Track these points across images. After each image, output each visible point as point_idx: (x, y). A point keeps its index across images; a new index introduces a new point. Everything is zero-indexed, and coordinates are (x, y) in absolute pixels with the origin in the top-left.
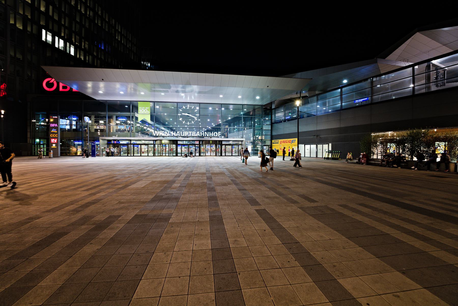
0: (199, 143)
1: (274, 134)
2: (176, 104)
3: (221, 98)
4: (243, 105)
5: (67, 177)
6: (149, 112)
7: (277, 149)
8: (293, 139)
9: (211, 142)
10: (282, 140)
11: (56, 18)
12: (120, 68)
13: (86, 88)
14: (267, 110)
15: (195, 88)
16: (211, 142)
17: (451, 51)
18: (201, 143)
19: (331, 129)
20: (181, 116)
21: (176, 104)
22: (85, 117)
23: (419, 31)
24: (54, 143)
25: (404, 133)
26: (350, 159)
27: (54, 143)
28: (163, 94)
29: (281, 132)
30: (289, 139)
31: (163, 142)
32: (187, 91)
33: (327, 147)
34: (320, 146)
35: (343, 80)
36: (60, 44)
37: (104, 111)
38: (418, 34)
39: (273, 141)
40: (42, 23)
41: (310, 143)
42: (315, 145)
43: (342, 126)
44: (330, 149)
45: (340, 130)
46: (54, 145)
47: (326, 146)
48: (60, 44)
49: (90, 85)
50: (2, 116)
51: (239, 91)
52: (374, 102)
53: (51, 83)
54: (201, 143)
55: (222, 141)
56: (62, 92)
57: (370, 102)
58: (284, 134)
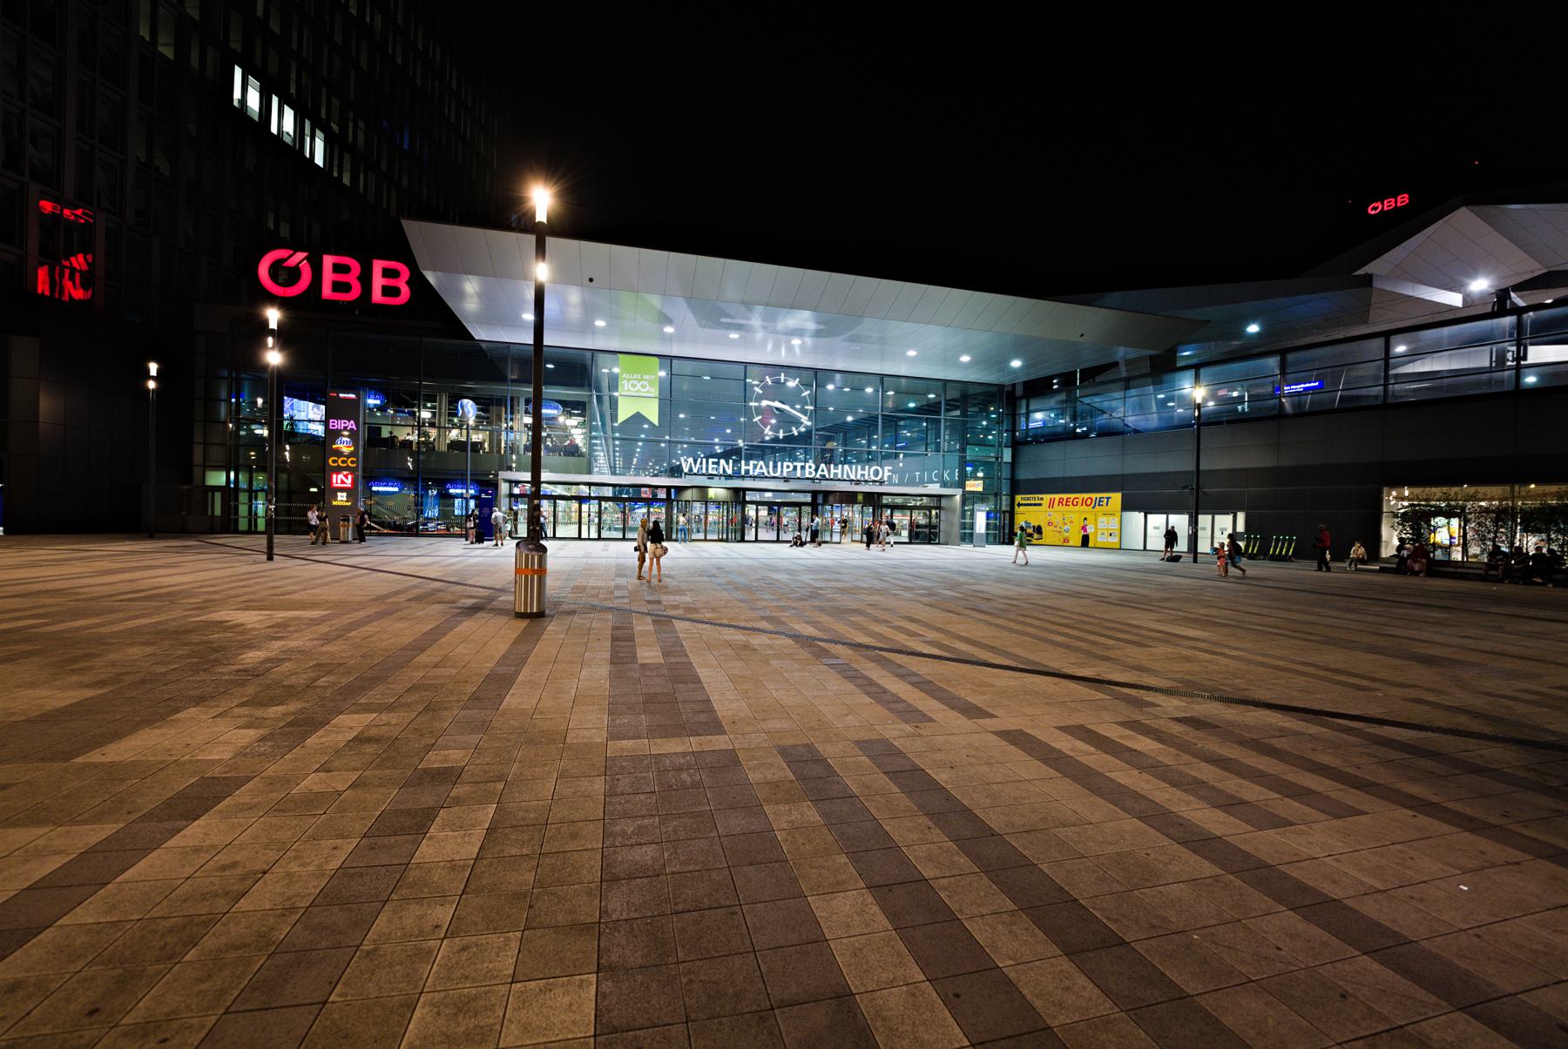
0: (669, 494)
1: (1023, 474)
2: (742, 367)
3: (604, 331)
6: (655, 392)
9: (860, 498)
11: (275, 26)
12: (454, 223)
13: (461, 294)
14: (1009, 398)
15: (803, 319)
16: (860, 498)
17: (1538, 269)
18: (820, 500)
20: (759, 410)
21: (742, 367)
22: (465, 401)
23: (1468, 203)
24: (342, 490)
25: (198, 438)
26: (1362, 561)
27: (342, 490)
28: (734, 336)
29: (1054, 472)
30: (1086, 496)
31: (712, 493)
32: (782, 328)
33: (1221, 528)
34: (1204, 520)
35: (1248, 324)
36: (285, 122)
38: (1463, 209)
39: (1018, 498)
40: (236, 46)
43: (1286, 461)
44: (1241, 528)
45: (1275, 475)
46: (342, 496)
47: (1224, 522)
48: (285, 122)
49: (471, 286)
50: (152, 385)
51: (931, 335)
52: (1391, 401)
53: (289, 268)
54: (820, 500)
56: (379, 306)
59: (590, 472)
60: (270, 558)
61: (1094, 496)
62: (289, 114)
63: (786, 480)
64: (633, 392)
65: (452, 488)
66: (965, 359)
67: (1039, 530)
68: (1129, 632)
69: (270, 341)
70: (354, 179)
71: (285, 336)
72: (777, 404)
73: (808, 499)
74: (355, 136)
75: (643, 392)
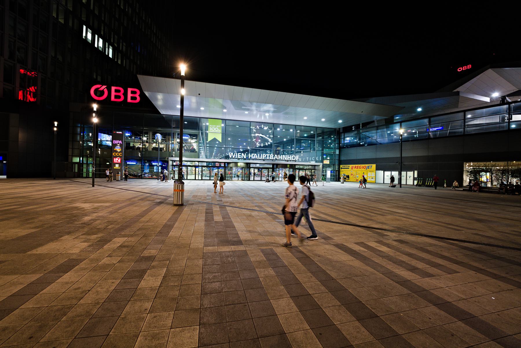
0: (225, 165)
1: (342, 158)
3: (204, 111)
4: (250, 122)
5: (103, 203)
6: (220, 131)
7: (347, 174)
8: (368, 165)
9: (288, 166)
10: (354, 165)
11: (97, 12)
12: (154, 76)
14: (338, 133)
15: (270, 107)
16: (288, 166)
18: (275, 167)
19: (418, 157)
20: (255, 137)
22: (158, 134)
23: (492, 67)
24: (117, 163)
26: (457, 187)
27: (117, 163)
28: (247, 112)
31: (239, 164)
32: (262, 110)
35: (418, 108)
36: (100, 43)
37: (170, 127)
38: (490, 72)
39: (341, 166)
40: (84, 19)
41: (391, 169)
42: (397, 172)
43: (431, 154)
44: (416, 176)
45: (427, 158)
46: (117, 166)
47: (410, 174)
48: (100, 43)
49: (160, 96)
50: (55, 129)
51: (312, 112)
52: (466, 133)
53: (101, 91)
54: (275, 167)
55: (250, 163)
57: (462, 134)
58: (356, 160)
60: (93, 186)
61: (366, 165)
62: (101, 41)
64: (213, 131)
65: (150, 162)
66: (323, 120)
69: (94, 115)
70: (122, 62)
71: (99, 113)
73: (271, 166)
75: (217, 131)
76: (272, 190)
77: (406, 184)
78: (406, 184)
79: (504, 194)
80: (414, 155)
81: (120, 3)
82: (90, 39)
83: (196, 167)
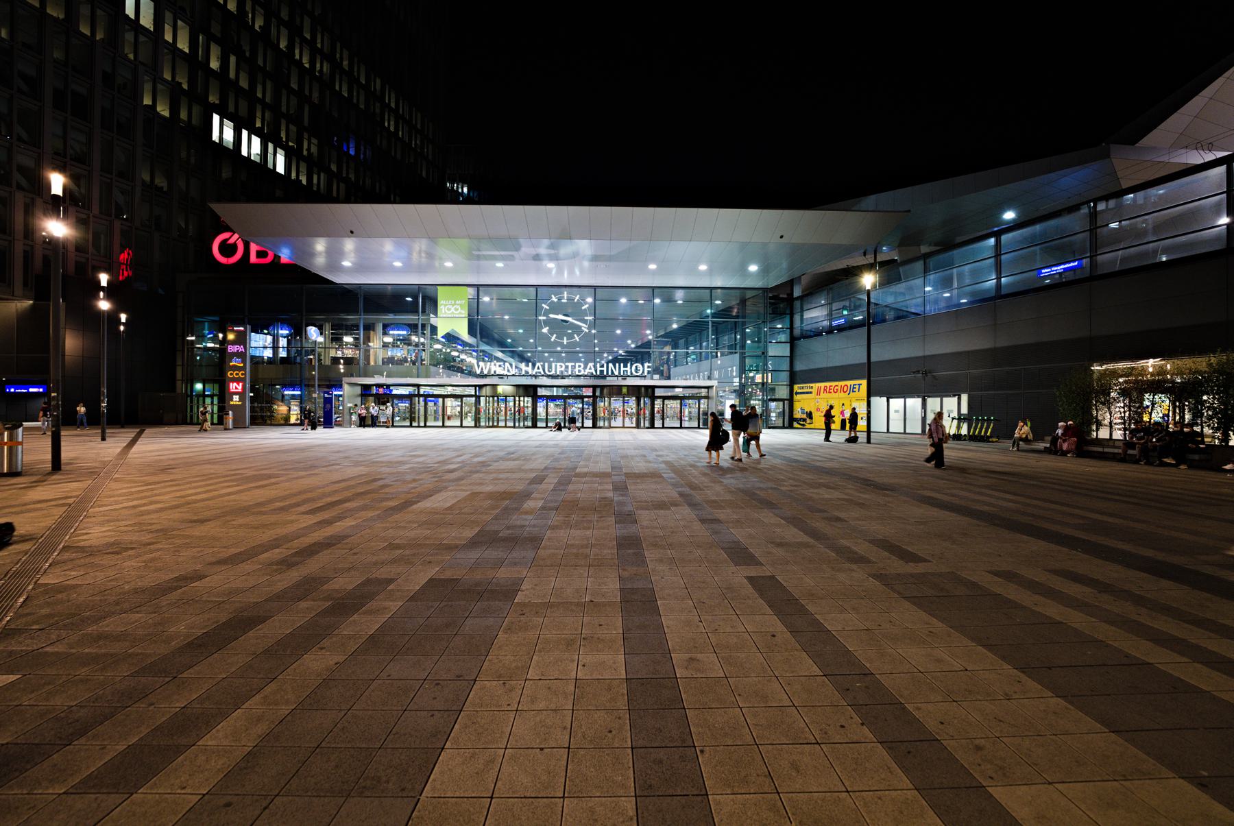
0: (594, 392)
1: (799, 367)
3: (654, 273)
4: (711, 289)
6: (465, 313)
9: (625, 390)
11: (244, 83)
12: (356, 202)
14: (779, 302)
15: (584, 246)
16: (625, 390)
20: (548, 322)
21: (533, 290)
24: (236, 393)
26: (1026, 440)
27: (236, 393)
28: (500, 265)
29: (819, 363)
31: (500, 390)
32: (562, 255)
33: (952, 407)
36: (252, 147)
39: (796, 387)
40: (213, 99)
41: (904, 393)
43: (1003, 342)
44: (964, 410)
45: (994, 356)
46: (236, 398)
48: (252, 147)
49: (320, 246)
50: (122, 328)
51: (702, 251)
55: (654, 387)
56: (255, 265)
57: (1087, 274)
59: (669, 378)
60: (103, 439)
61: (849, 383)
62: (256, 141)
63: (596, 377)
64: (449, 314)
65: (308, 388)
66: (703, 267)
67: (810, 415)
68: (151, 503)
69: (102, 294)
70: (309, 179)
71: (111, 292)
72: (561, 317)
73: (472, 391)
74: (309, 150)
75: (456, 314)
76: (684, 448)
77: (905, 433)
78: (905, 433)
79: (1137, 462)
80: (948, 351)
81: (341, 58)
82: (231, 139)
83: (682, 399)
